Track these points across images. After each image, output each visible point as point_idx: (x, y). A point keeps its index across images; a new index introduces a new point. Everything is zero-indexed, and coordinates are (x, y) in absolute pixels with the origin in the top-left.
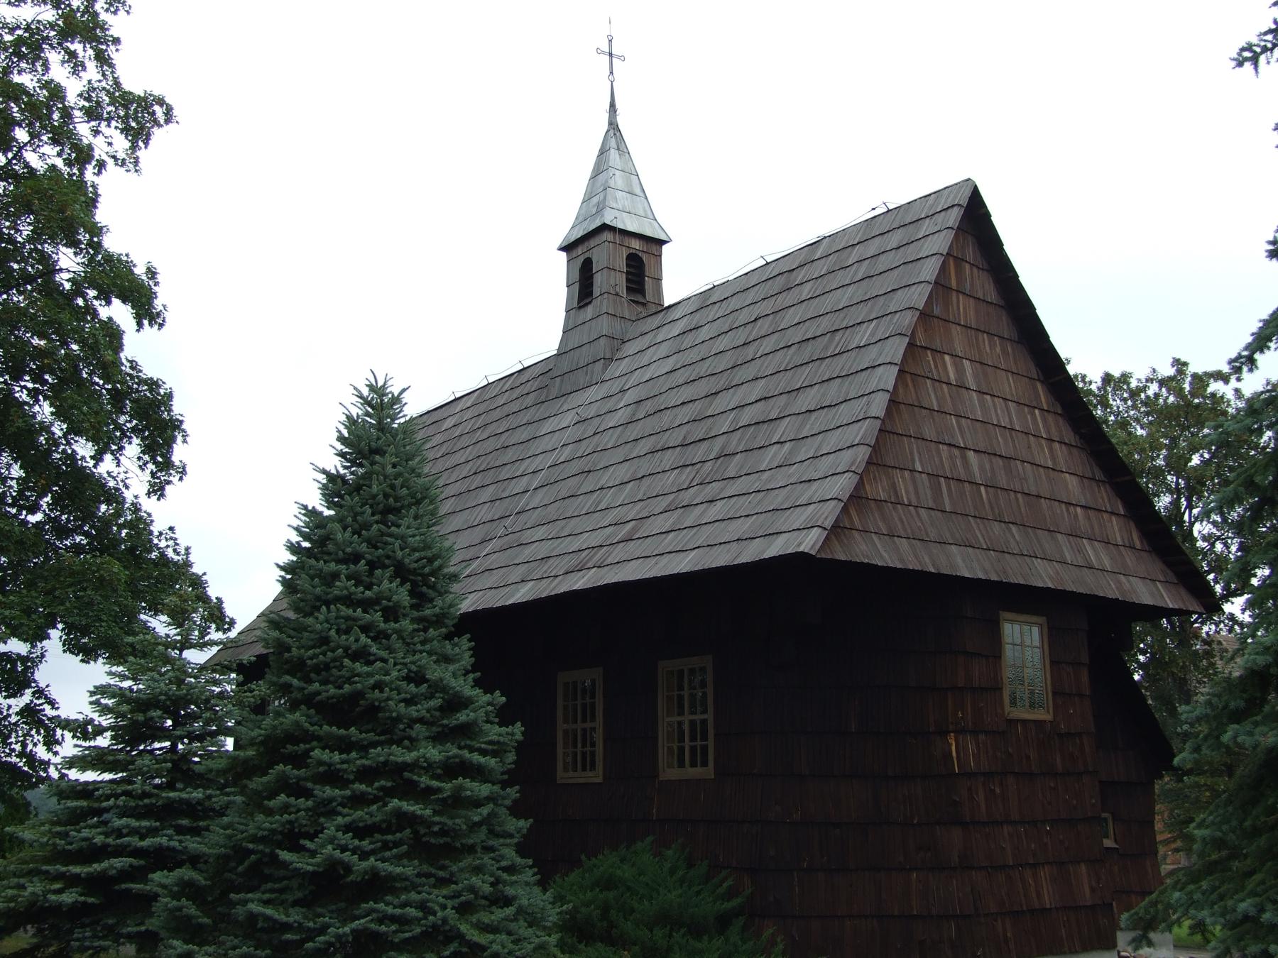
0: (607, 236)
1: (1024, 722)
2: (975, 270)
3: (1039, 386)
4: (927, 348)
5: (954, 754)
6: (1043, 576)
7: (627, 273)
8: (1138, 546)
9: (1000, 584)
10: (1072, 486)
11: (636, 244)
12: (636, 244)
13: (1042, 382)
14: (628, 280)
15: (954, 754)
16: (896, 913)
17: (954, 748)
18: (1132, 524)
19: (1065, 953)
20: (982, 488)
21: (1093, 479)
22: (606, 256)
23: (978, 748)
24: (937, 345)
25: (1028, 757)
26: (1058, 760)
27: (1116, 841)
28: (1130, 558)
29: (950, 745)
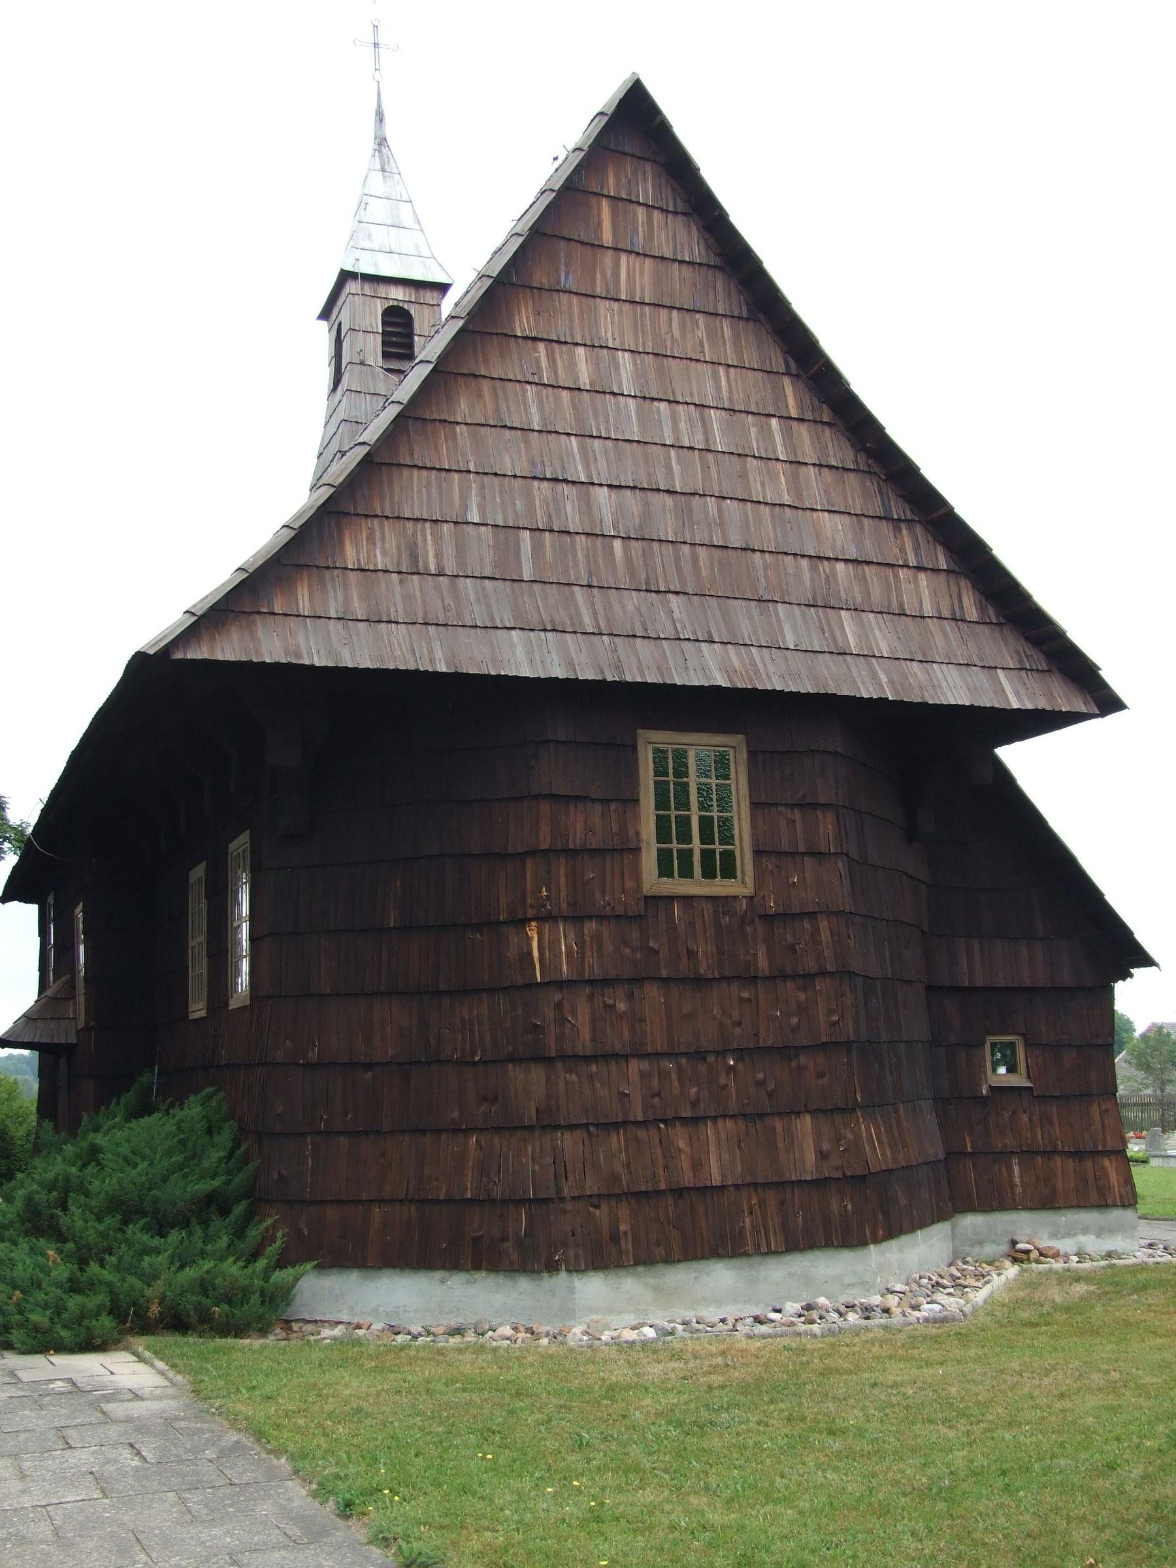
0: (352, 287)
1: (687, 900)
2: (656, 215)
3: (787, 382)
4: (534, 339)
5: (536, 954)
6: (709, 668)
7: (384, 333)
8: (972, 613)
9: (817, 695)
10: (836, 533)
11: (398, 294)
12: (398, 294)
13: (795, 377)
14: (384, 343)
15: (536, 954)
16: (442, 1197)
17: (535, 944)
18: (965, 585)
19: (747, 1255)
20: (617, 544)
21: (888, 519)
22: (366, 313)
23: (581, 943)
24: (560, 329)
25: (691, 954)
26: (761, 954)
27: (1029, 1077)
28: (944, 637)
29: (530, 939)
